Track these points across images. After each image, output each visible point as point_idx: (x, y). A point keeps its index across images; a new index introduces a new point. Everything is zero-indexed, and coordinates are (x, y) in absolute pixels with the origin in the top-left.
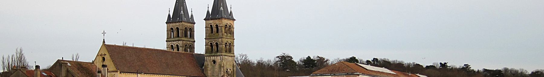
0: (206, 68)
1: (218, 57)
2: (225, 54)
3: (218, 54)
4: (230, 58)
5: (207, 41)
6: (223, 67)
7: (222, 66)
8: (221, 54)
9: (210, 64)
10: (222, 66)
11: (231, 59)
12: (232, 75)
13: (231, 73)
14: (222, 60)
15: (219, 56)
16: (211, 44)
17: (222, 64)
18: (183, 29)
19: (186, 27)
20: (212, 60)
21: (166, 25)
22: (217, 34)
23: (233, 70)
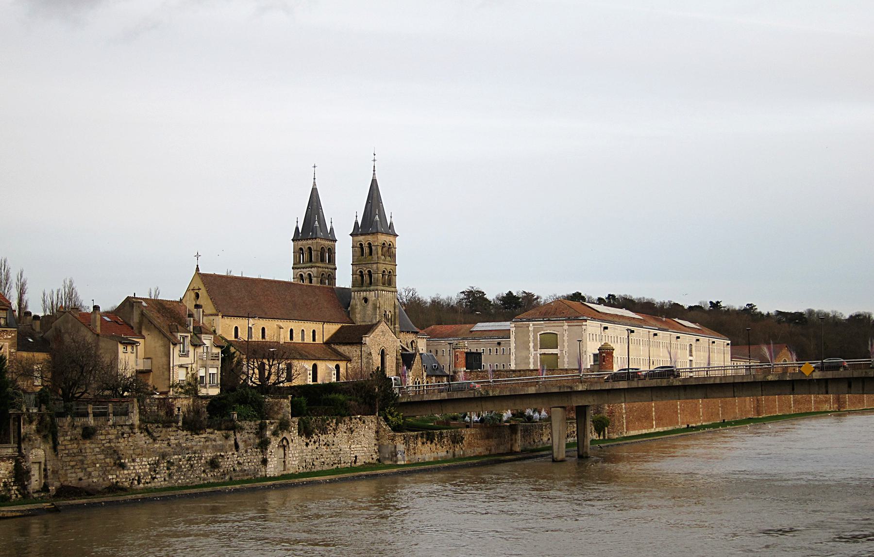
0: (353, 309)
1: (371, 293)
2: (382, 288)
3: (372, 288)
4: (390, 295)
5: (355, 268)
6: (379, 308)
7: (378, 306)
8: (376, 287)
9: (358, 303)
10: (378, 306)
11: (391, 295)
12: (393, 320)
13: (391, 317)
14: (378, 297)
15: (373, 291)
16: (361, 272)
17: (378, 304)
18: (318, 249)
19: (330, 247)
20: (362, 297)
21: (292, 243)
22: (370, 257)
23: (395, 313)
